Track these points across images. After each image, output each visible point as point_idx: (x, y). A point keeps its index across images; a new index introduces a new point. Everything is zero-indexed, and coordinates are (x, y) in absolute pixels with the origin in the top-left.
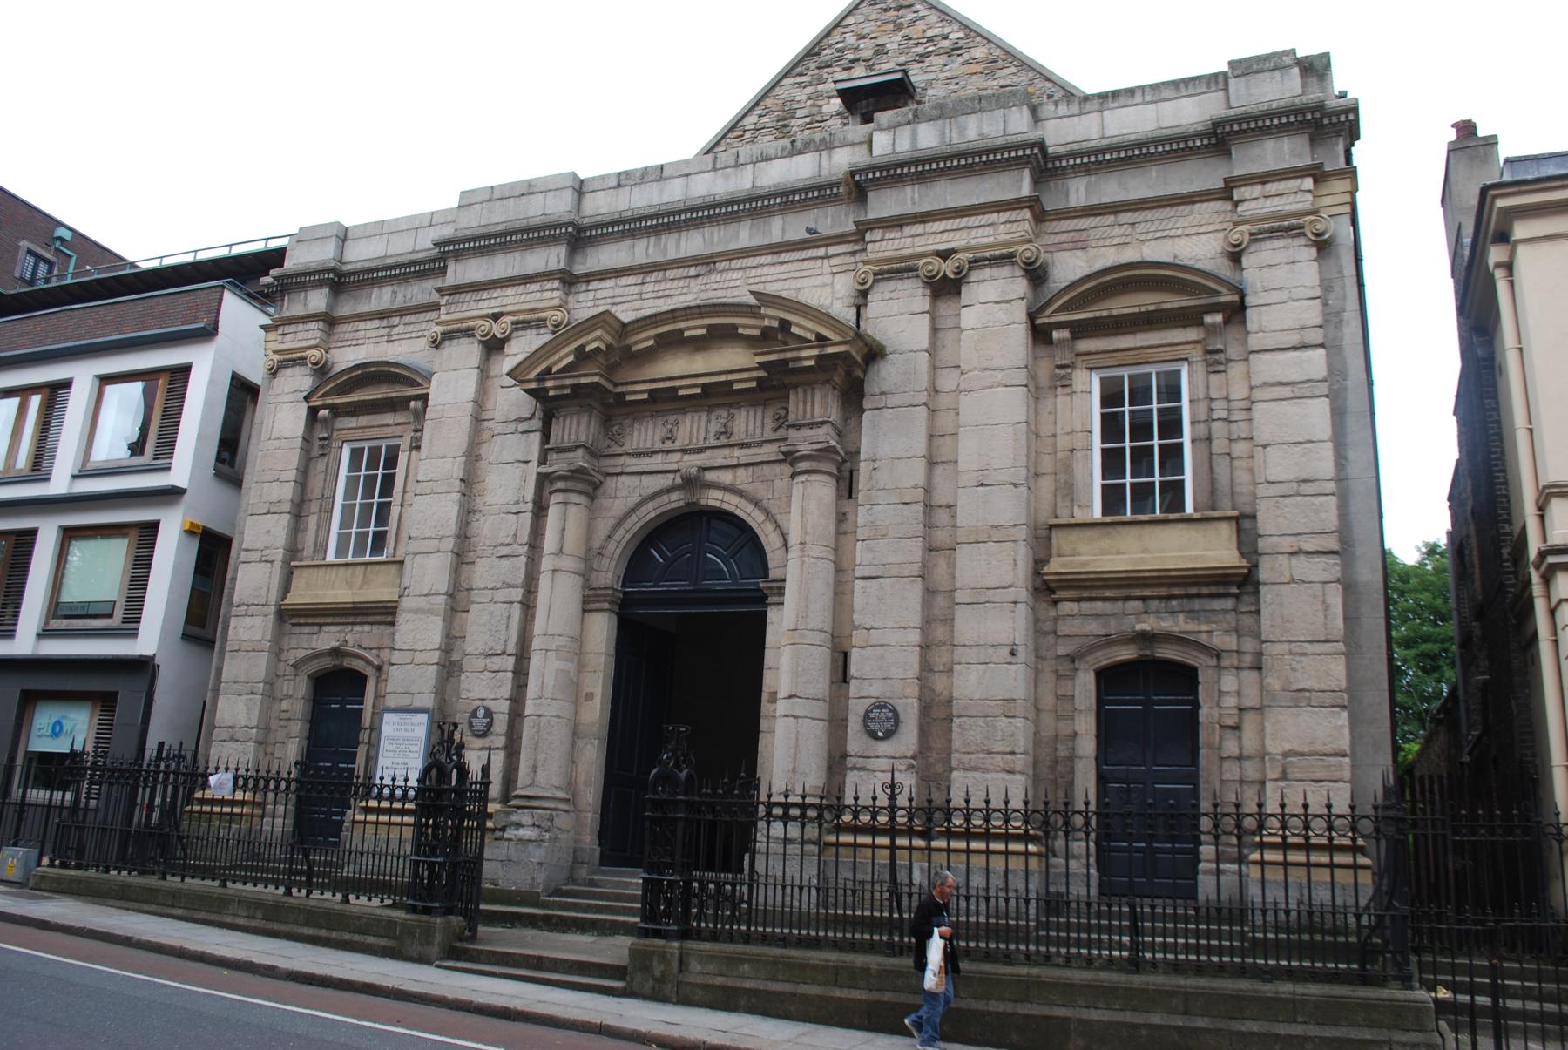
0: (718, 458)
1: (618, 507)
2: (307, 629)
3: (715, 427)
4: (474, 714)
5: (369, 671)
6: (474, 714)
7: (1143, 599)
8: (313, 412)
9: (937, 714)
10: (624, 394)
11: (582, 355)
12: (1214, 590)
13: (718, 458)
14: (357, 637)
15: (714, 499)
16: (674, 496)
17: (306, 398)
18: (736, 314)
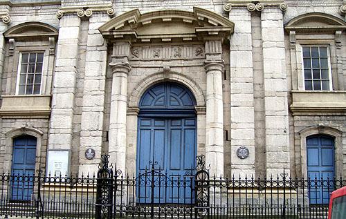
0: (176, 63)
1: (137, 79)
2: (9, 121)
3: (174, 53)
4: (87, 151)
5: (38, 136)
6: (87, 151)
7: (320, 116)
8: (6, 40)
9: (262, 151)
10: (141, 39)
11: (127, 23)
12: (340, 114)
13: (176, 63)
14: (35, 125)
15: (175, 78)
16: (159, 76)
17: (3, 34)
18: (183, 15)
